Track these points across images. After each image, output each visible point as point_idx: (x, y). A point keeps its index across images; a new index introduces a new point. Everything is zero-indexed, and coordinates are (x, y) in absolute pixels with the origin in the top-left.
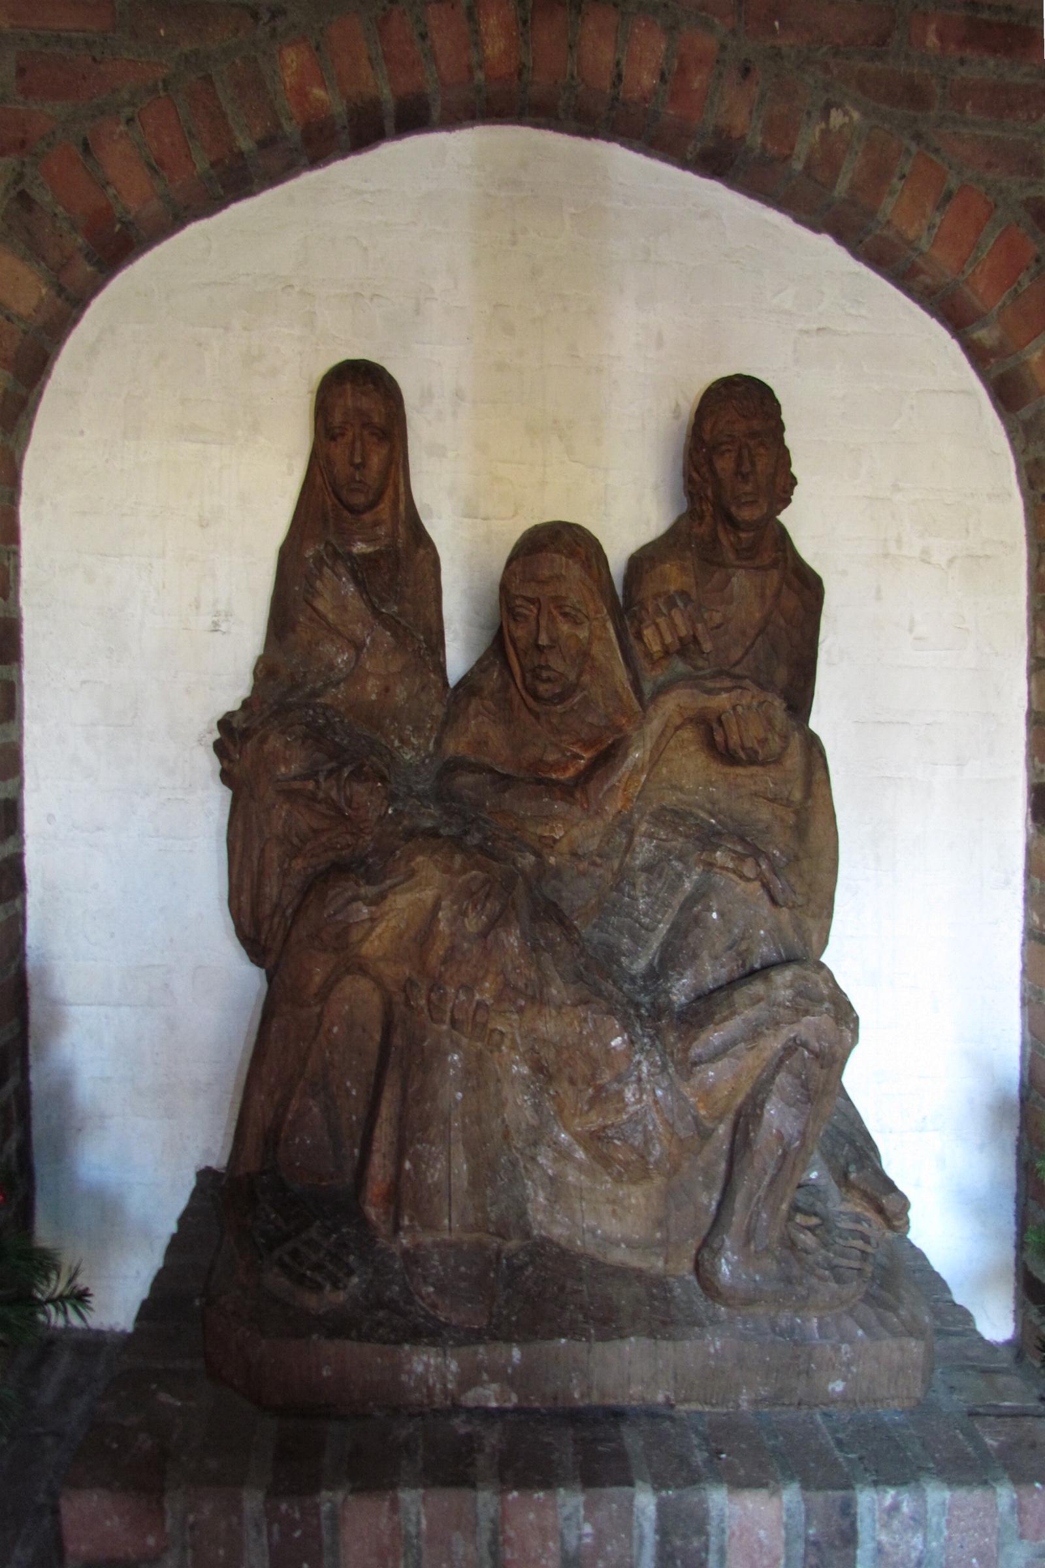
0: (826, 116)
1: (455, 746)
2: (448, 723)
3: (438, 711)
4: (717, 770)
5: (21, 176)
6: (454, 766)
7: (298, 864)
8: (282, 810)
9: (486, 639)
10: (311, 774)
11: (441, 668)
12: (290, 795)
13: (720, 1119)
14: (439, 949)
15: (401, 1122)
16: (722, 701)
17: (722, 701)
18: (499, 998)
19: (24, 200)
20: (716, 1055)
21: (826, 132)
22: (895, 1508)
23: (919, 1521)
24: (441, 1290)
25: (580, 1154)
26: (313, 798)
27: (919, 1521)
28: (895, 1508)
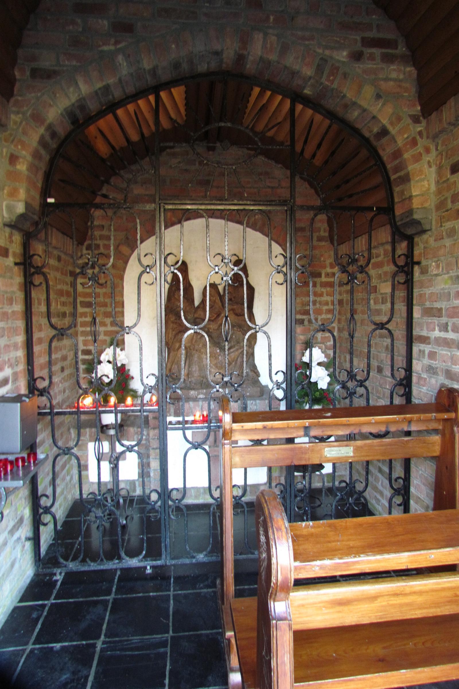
0: (255, 216)
1: (196, 316)
2: (195, 312)
3: (194, 311)
4: (236, 317)
5: (126, 235)
6: (196, 318)
7: (174, 332)
8: (172, 325)
9: (201, 300)
10: (176, 319)
11: (194, 304)
12: (173, 322)
13: (233, 362)
14: (194, 341)
15: (257, 118)
16: (235, 307)
17: (235, 307)
18: (202, 346)
19: (127, 238)
20: (410, 593)
21: (255, 219)
22: (252, 403)
23: (256, 405)
24: (195, 384)
25: (214, 367)
26: (176, 323)
27: (256, 405)
28: (252, 403)
